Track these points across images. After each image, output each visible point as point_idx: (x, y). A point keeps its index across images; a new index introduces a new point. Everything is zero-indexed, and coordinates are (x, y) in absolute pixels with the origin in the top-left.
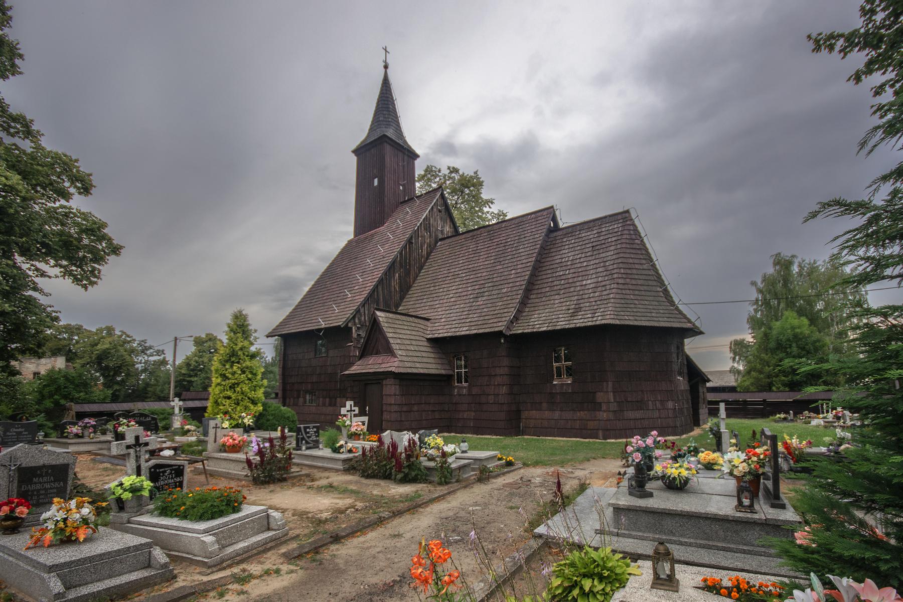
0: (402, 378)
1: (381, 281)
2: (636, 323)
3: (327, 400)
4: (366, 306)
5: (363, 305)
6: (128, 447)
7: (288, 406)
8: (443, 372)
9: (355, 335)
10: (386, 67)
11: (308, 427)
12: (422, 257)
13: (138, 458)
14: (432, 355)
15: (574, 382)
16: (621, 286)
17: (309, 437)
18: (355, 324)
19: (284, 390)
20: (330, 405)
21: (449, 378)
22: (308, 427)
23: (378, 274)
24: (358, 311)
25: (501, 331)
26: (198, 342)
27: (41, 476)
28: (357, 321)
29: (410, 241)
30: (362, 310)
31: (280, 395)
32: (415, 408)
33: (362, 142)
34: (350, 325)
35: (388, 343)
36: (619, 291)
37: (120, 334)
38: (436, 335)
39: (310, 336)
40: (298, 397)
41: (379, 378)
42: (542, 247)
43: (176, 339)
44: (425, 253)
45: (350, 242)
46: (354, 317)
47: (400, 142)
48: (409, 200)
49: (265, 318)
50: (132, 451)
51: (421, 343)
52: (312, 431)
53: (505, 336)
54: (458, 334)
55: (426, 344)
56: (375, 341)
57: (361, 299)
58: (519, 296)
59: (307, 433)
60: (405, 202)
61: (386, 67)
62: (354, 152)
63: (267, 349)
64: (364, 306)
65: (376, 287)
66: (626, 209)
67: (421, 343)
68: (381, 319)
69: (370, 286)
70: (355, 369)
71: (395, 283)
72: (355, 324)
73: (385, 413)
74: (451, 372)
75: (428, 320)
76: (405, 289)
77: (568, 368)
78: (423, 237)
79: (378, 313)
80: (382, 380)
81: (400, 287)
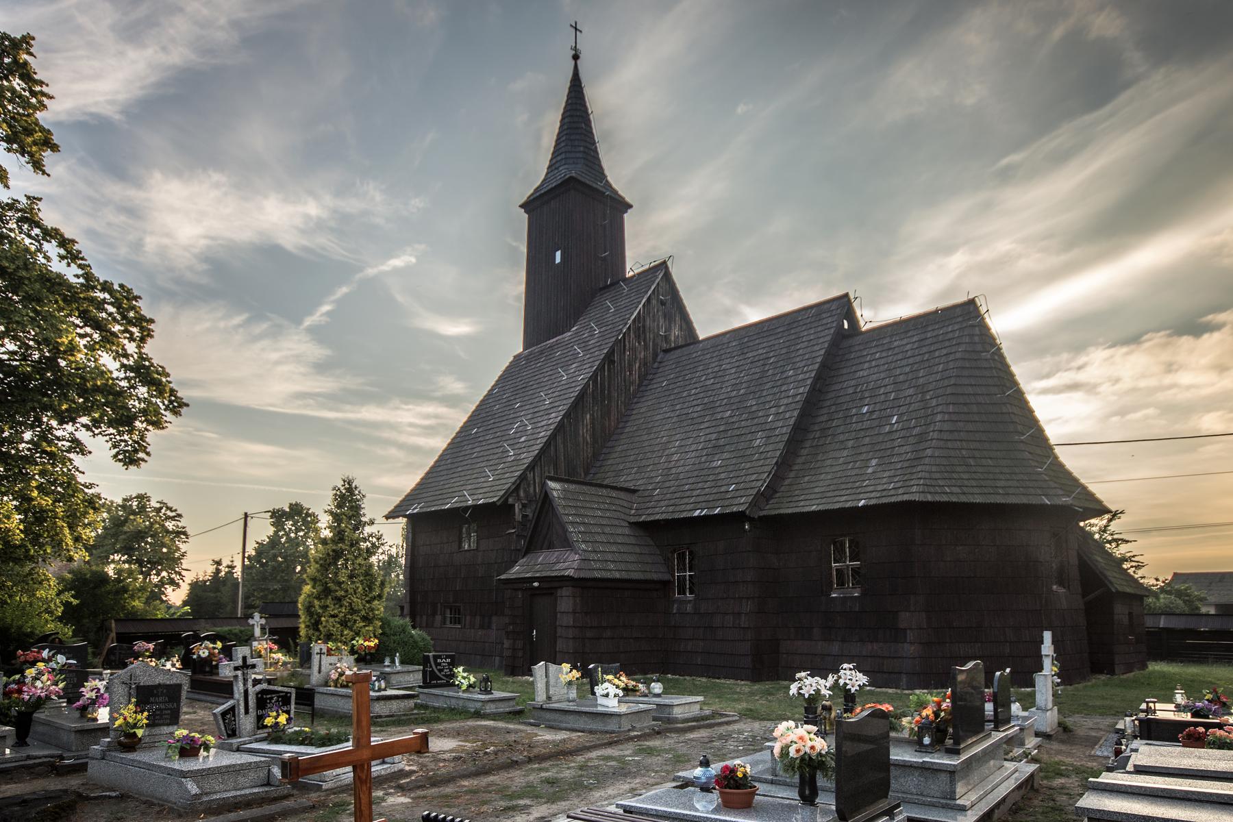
0: (580, 584)
1: (560, 428)
2: (963, 499)
3: (478, 618)
4: (537, 470)
5: (531, 467)
6: (236, 669)
7: (421, 628)
8: (655, 577)
9: (518, 517)
10: (576, 57)
11: (440, 657)
12: (632, 383)
13: (245, 681)
14: (638, 550)
15: (863, 594)
16: (945, 436)
17: (440, 671)
18: (519, 499)
19: (413, 603)
20: (482, 627)
21: (666, 584)
22: (440, 657)
23: (556, 417)
24: (523, 478)
25: (743, 513)
26: (278, 517)
27: (157, 695)
28: (522, 494)
29: (609, 358)
30: (530, 476)
31: (406, 611)
32: (608, 633)
33: (536, 190)
34: (511, 501)
35: (565, 531)
36: (941, 444)
37: (158, 505)
38: (643, 518)
39: (454, 518)
40: (434, 614)
41: (551, 585)
42: (824, 366)
43: (246, 515)
44: (636, 376)
45: (517, 358)
46: (517, 488)
47: (599, 186)
48: (612, 284)
49: (388, 483)
50: (239, 673)
51: (619, 531)
52: (445, 662)
53: (751, 520)
54: (676, 516)
55: (627, 531)
56: (542, 528)
57: (527, 458)
58: (778, 453)
59: (437, 664)
60: (606, 287)
61: (576, 57)
62: (521, 206)
63: (390, 538)
64: (533, 468)
65: (553, 437)
66: (971, 297)
67: (619, 531)
68: (555, 494)
69: (544, 435)
70: (516, 571)
71: (585, 432)
72: (519, 499)
73: (559, 642)
74: (667, 577)
75: (634, 491)
76: (604, 439)
77: (855, 571)
78: (633, 349)
79: (551, 484)
80: (556, 588)
81: (593, 435)
